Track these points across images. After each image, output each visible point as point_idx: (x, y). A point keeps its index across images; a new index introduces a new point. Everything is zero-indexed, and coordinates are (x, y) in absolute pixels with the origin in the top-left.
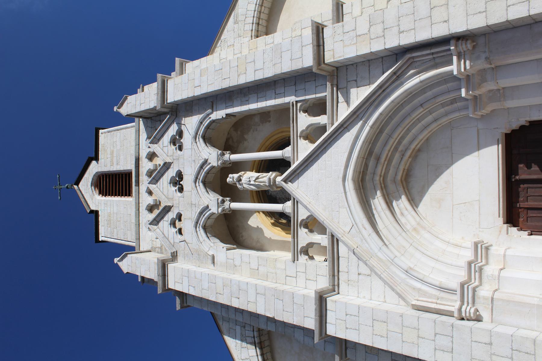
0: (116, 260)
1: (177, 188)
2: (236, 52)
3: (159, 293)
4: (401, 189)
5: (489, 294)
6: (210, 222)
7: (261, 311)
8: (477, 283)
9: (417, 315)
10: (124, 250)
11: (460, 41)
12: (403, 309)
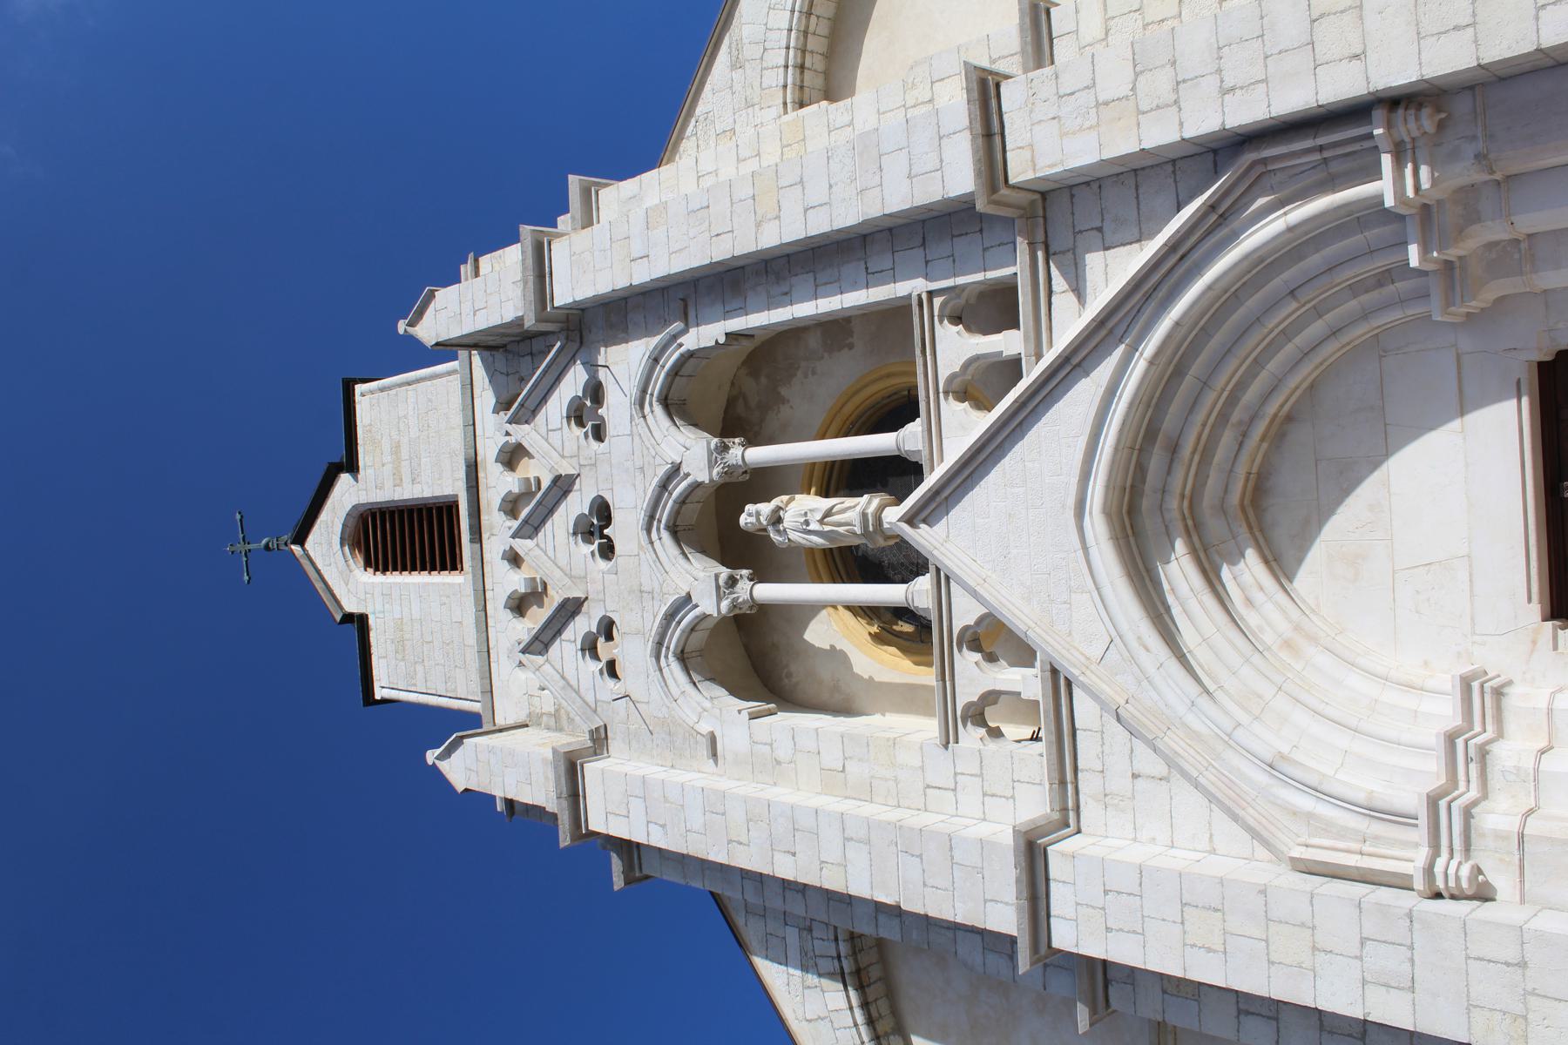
0: (431, 756)
1: (595, 546)
2: (744, 153)
3: (562, 845)
4: (1243, 531)
5: (1511, 824)
6: (698, 639)
7: (859, 888)
8: (1474, 793)
9: (1308, 888)
10: (456, 724)
11: (1401, 112)
12: (1265, 871)
